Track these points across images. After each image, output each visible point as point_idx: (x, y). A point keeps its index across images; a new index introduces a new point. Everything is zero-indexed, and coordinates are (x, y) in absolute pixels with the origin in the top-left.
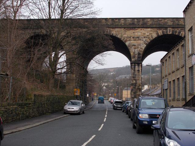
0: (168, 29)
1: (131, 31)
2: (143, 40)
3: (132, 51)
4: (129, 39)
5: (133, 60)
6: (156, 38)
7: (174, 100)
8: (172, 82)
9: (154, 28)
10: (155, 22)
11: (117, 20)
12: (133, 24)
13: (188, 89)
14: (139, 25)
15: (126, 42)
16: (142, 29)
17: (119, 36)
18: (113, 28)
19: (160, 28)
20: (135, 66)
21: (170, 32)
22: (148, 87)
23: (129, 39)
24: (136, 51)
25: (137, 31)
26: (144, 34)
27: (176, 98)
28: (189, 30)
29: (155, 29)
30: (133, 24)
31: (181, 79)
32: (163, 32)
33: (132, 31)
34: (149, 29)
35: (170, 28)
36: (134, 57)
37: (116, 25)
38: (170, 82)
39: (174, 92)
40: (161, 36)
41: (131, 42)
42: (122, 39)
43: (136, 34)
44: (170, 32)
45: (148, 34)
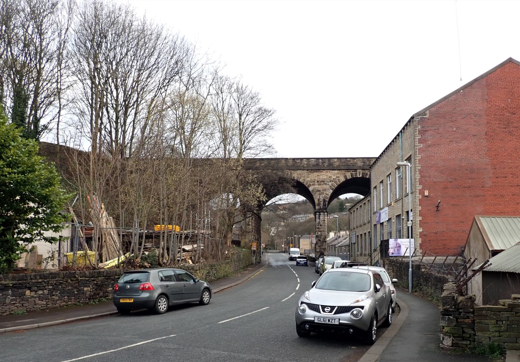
0: (358, 171)
1: (315, 174)
2: (329, 185)
3: (316, 197)
4: (313, 183)
5: (317, 207)
6: (343, 183)
7: (361, 254)
8: (359, 236)
9: (341, 170)
10: (343, 163)
11: (299, 161)
12: (317, 165)
13: (373, 245)
14: (324, 166)
15: (309, 187)
16: (328, 171)
17: (301, 180)
18: (294, 170)
19: (348, 170)
20: (320, 215)
21: (360, 175)
22: (335, 235)
23: (313, 183)
24: (321, 197)
25: (322, 173)
26: (330, 177)
27: (363, 253)
28: (374, 188)
29: (343, 172)
30: (317, 165)
31: (367, 234)
32: (352, 175)
33: (316, 174)
34: (336, 172)
35: (360, 170)
36: (319, 204)
37: (297, 166)
38: (358, 236)
39: (362, 247)
40: (350, 179)
41: (316, 186)
42: (305, 184)
43: (321, 177)
44: (360, 175)
45: (335, 177)
